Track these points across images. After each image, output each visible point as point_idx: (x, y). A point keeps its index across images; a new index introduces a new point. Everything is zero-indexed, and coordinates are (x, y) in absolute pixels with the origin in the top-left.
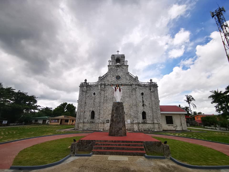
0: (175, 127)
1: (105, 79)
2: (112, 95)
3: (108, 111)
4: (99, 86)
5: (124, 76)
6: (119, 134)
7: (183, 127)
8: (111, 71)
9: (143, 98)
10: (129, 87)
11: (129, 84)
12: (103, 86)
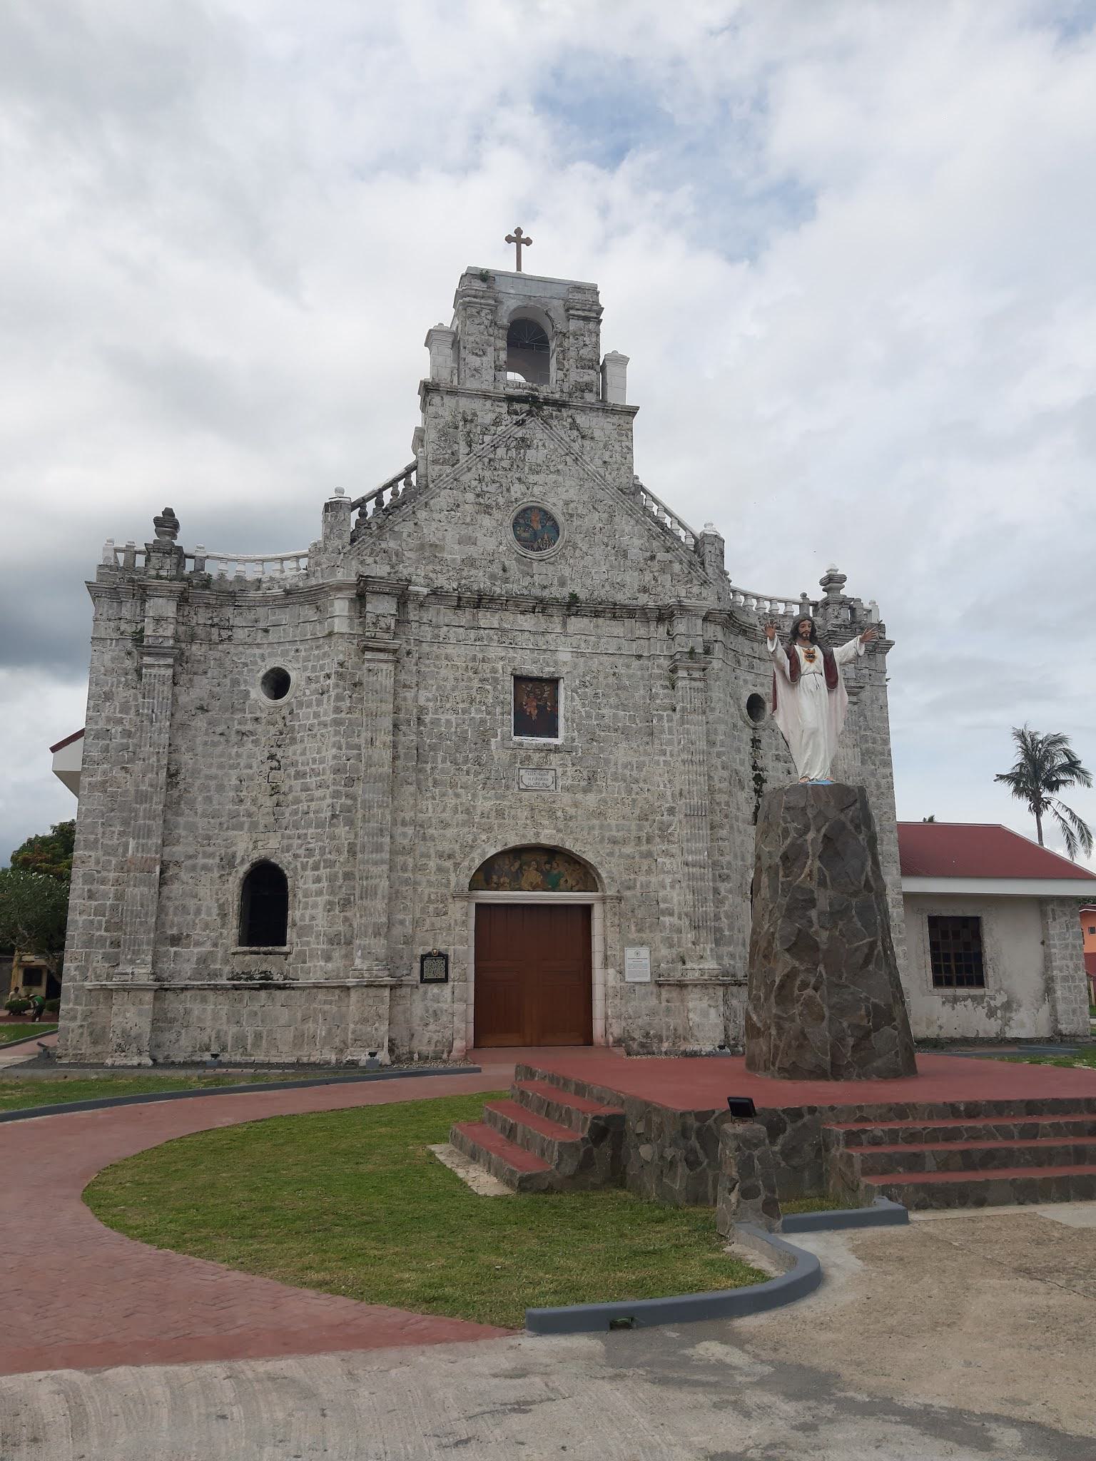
0: (999, 1013)
1: (397, 535)
2: (472, 701)
3: (440, 869)
4: (340, 607)
5: (594, 519)
6: (878, 1063)
7: (1061, 1007)
8: (463, 449)
9: (755, 742)
10: (641, 631)
11: (643, 599)
12: (382, 607)
